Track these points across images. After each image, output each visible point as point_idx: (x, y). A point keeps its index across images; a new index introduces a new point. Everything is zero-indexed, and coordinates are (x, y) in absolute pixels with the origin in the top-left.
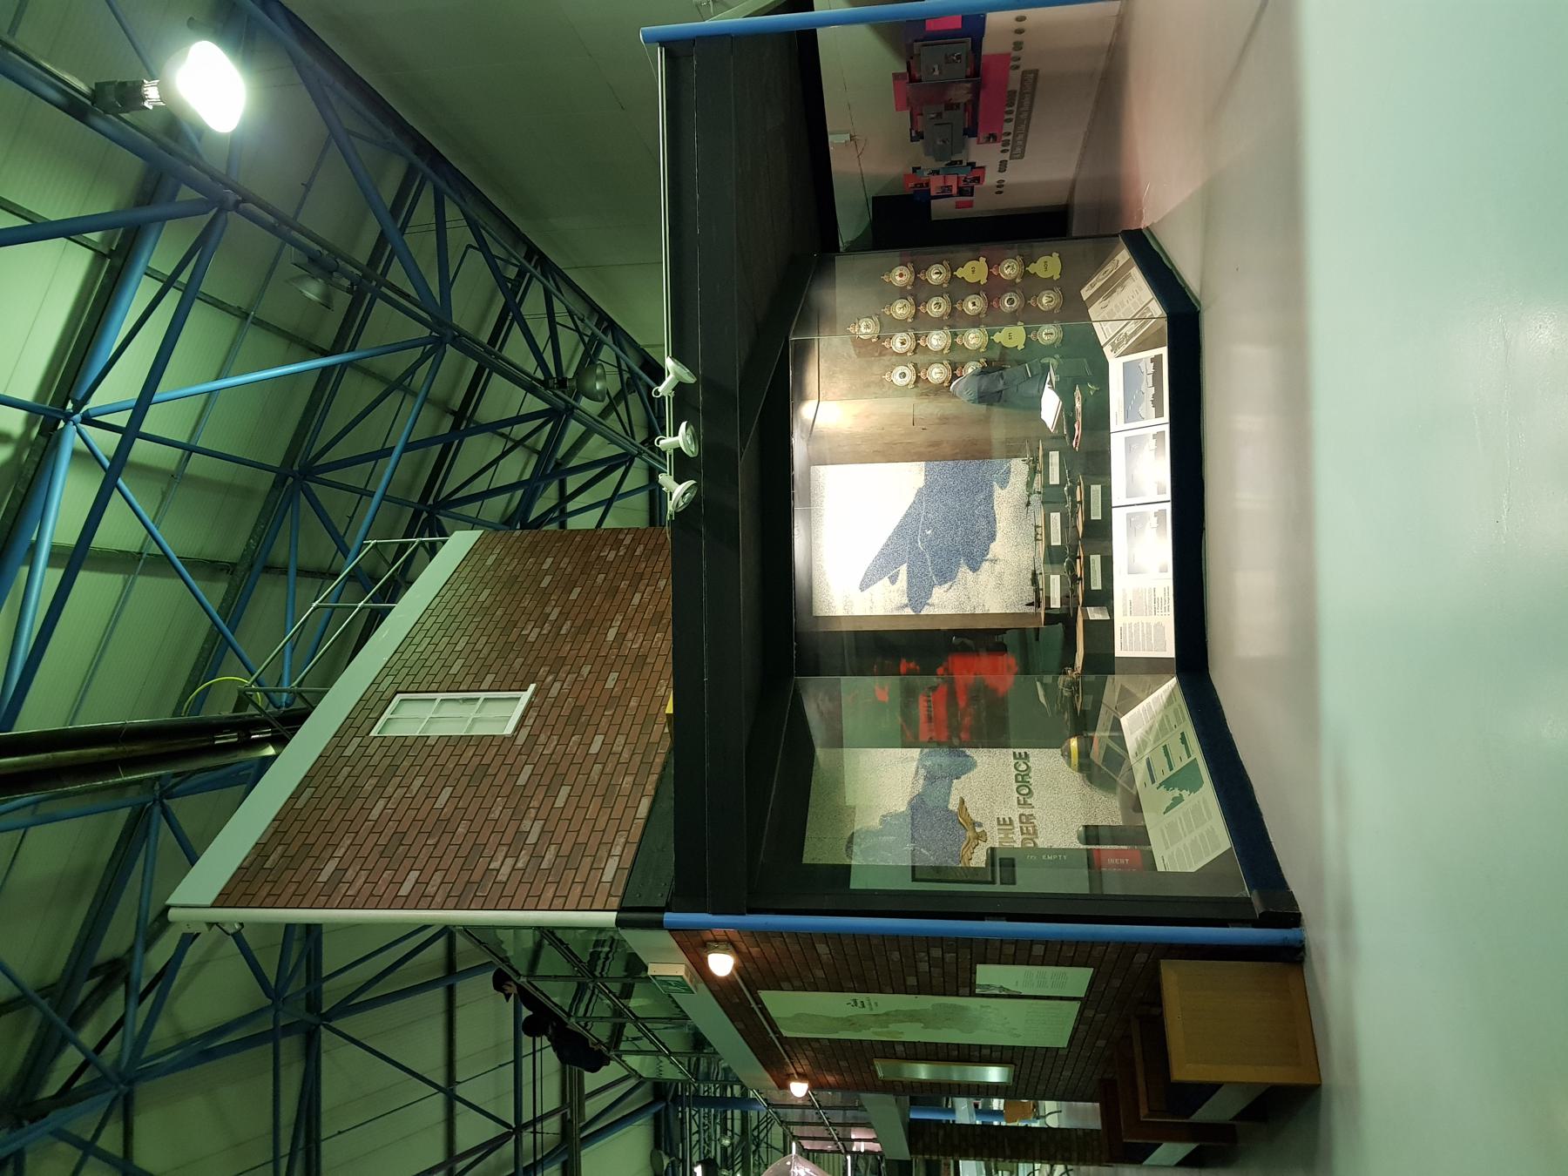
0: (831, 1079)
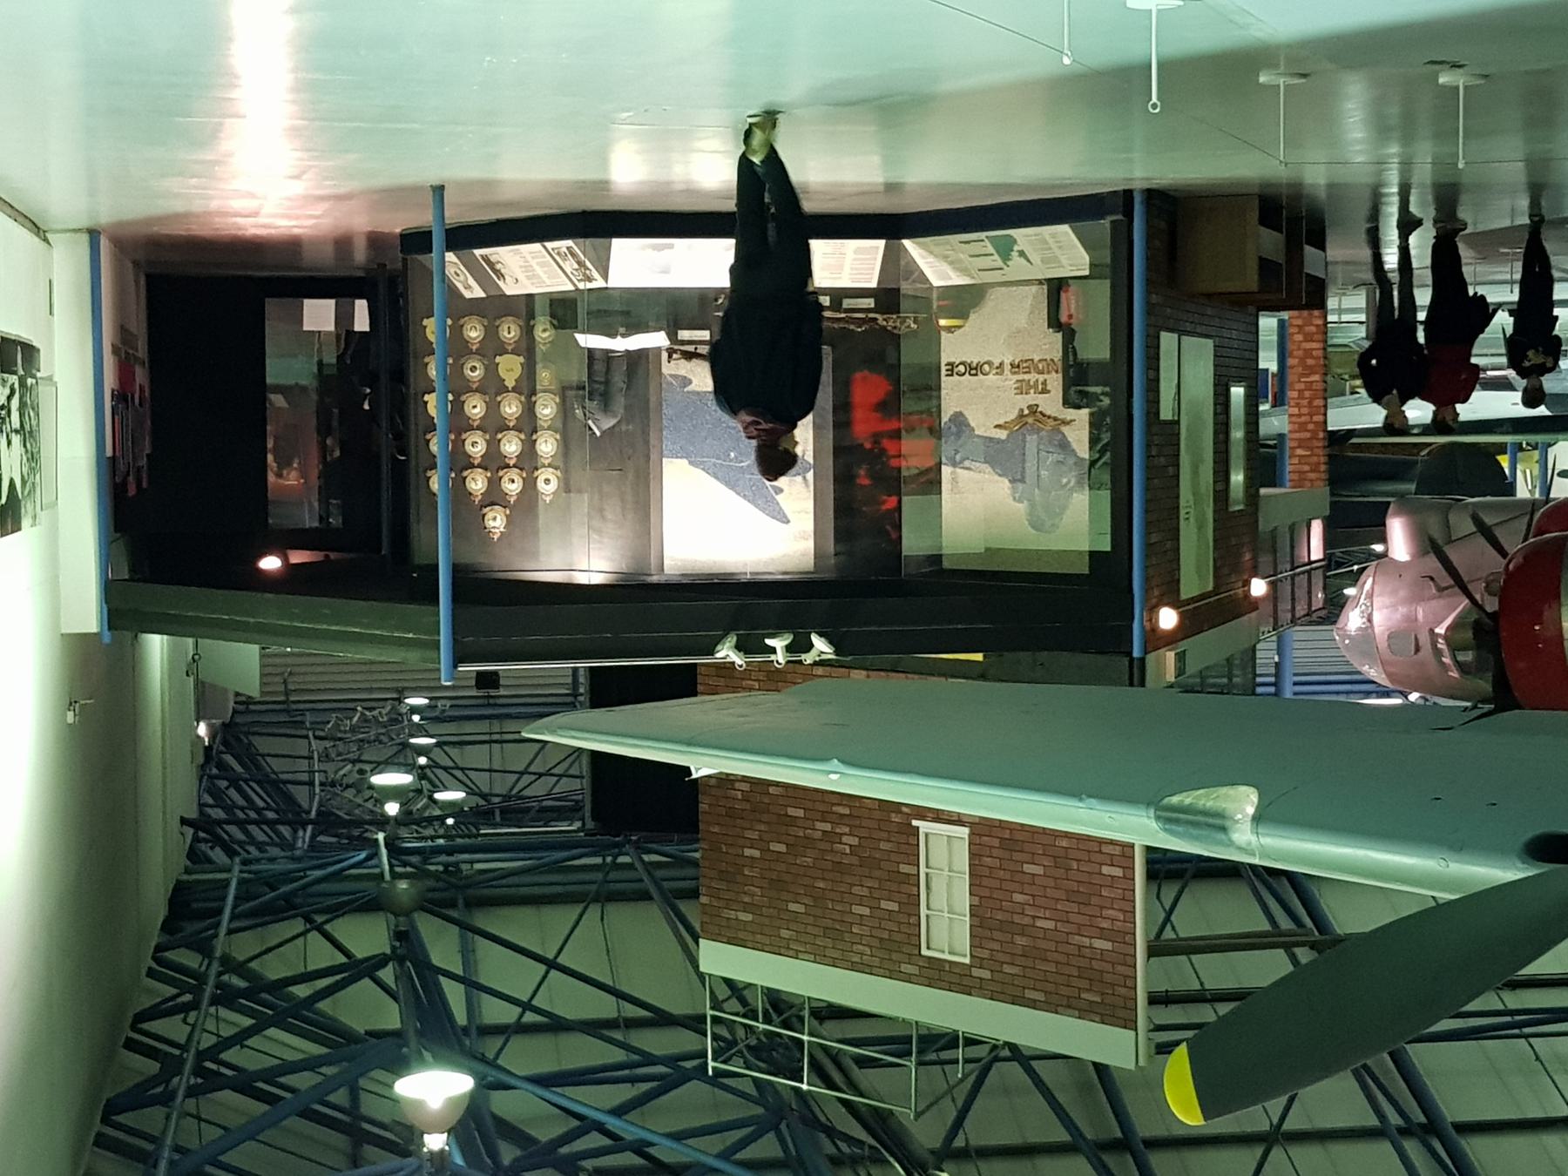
0: (1247, 556)
